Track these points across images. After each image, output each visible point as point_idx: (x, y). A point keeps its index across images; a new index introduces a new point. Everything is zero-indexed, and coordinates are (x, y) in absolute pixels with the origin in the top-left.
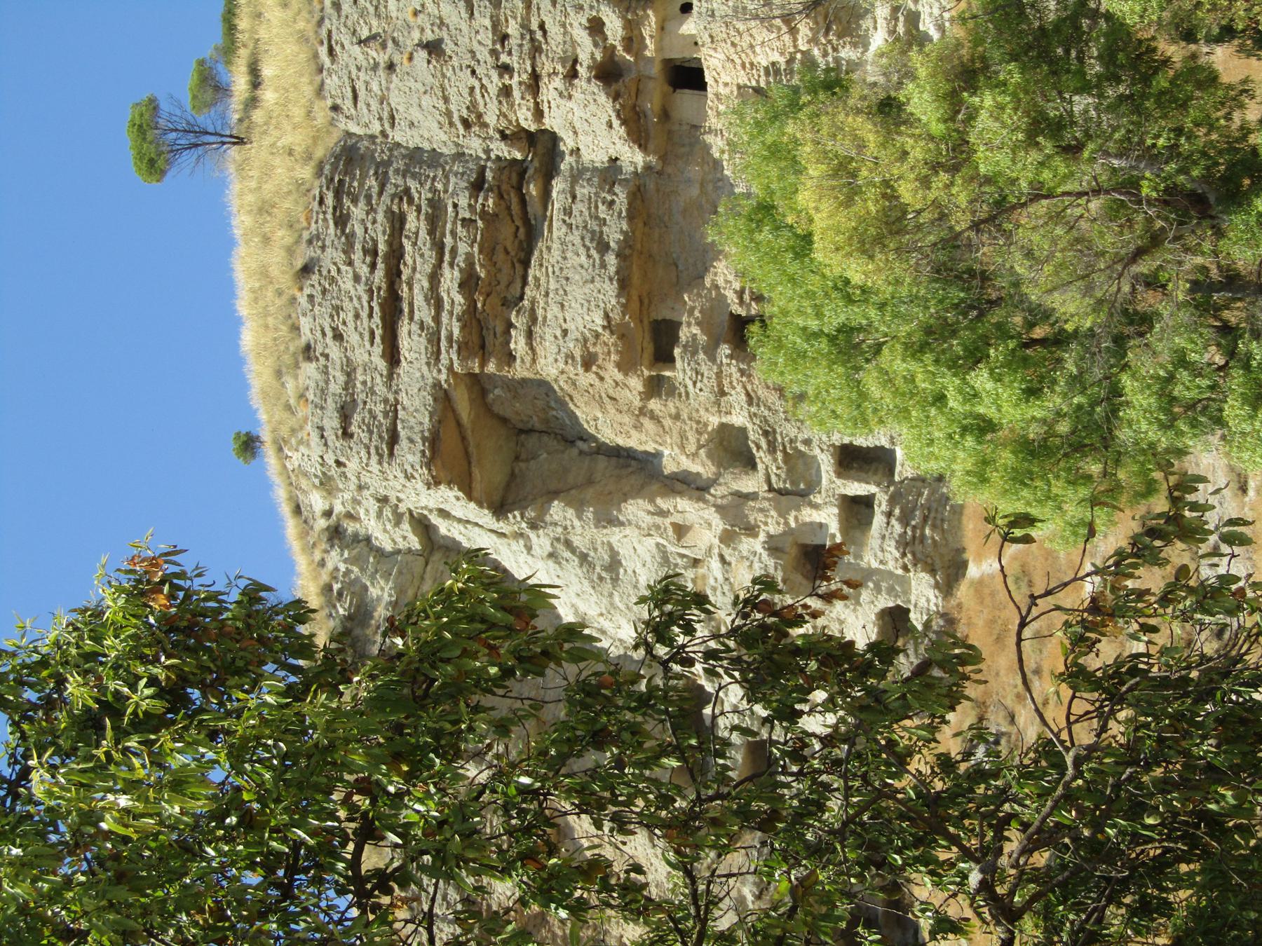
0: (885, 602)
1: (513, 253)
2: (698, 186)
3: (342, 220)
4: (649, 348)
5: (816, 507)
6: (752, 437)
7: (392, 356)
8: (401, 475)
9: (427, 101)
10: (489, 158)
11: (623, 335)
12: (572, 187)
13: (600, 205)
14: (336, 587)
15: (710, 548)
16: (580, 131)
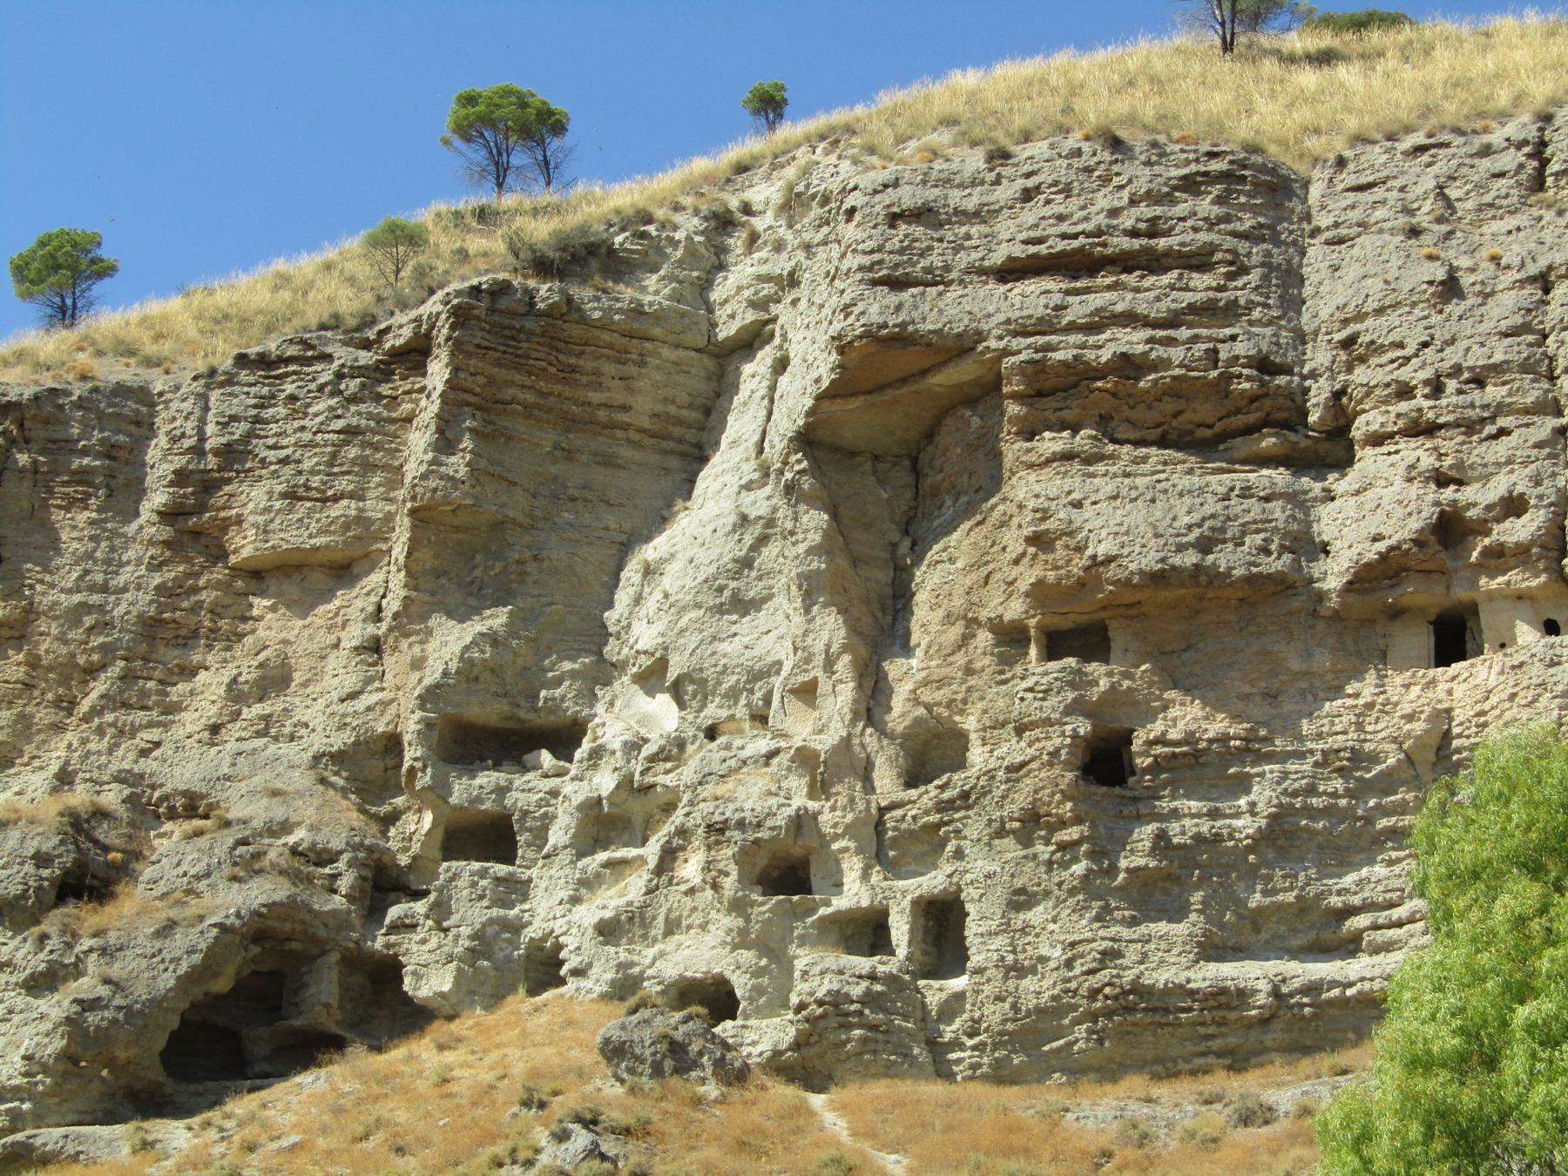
0: (741, 985)
1: (1175, 423)
2: (1304, 667)
3: (1191, 185)
4: (1065, 624)
5: (865, 876)
6: (955, 777)
7: (1011, 272)
8: (847, 298)
9: (1374, 286)
10: (1304, 378)
11: (1084, 585)
12: (1281, 496)
13: (1262, 535)
14: (651, 229)
15: (785, 736)
16: (1361, 498)
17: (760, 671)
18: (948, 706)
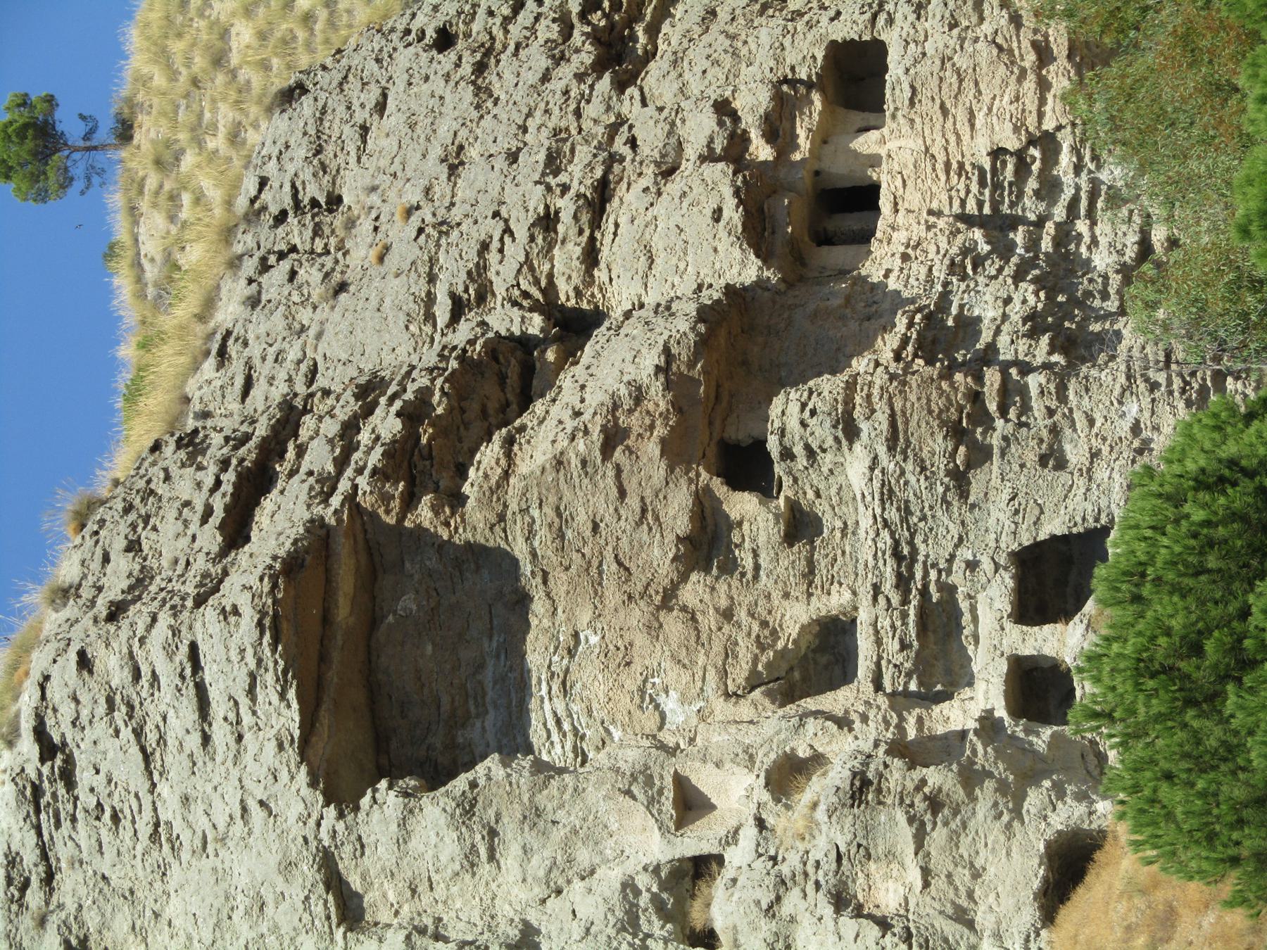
17: (626, 913)
18: (762, 648)
